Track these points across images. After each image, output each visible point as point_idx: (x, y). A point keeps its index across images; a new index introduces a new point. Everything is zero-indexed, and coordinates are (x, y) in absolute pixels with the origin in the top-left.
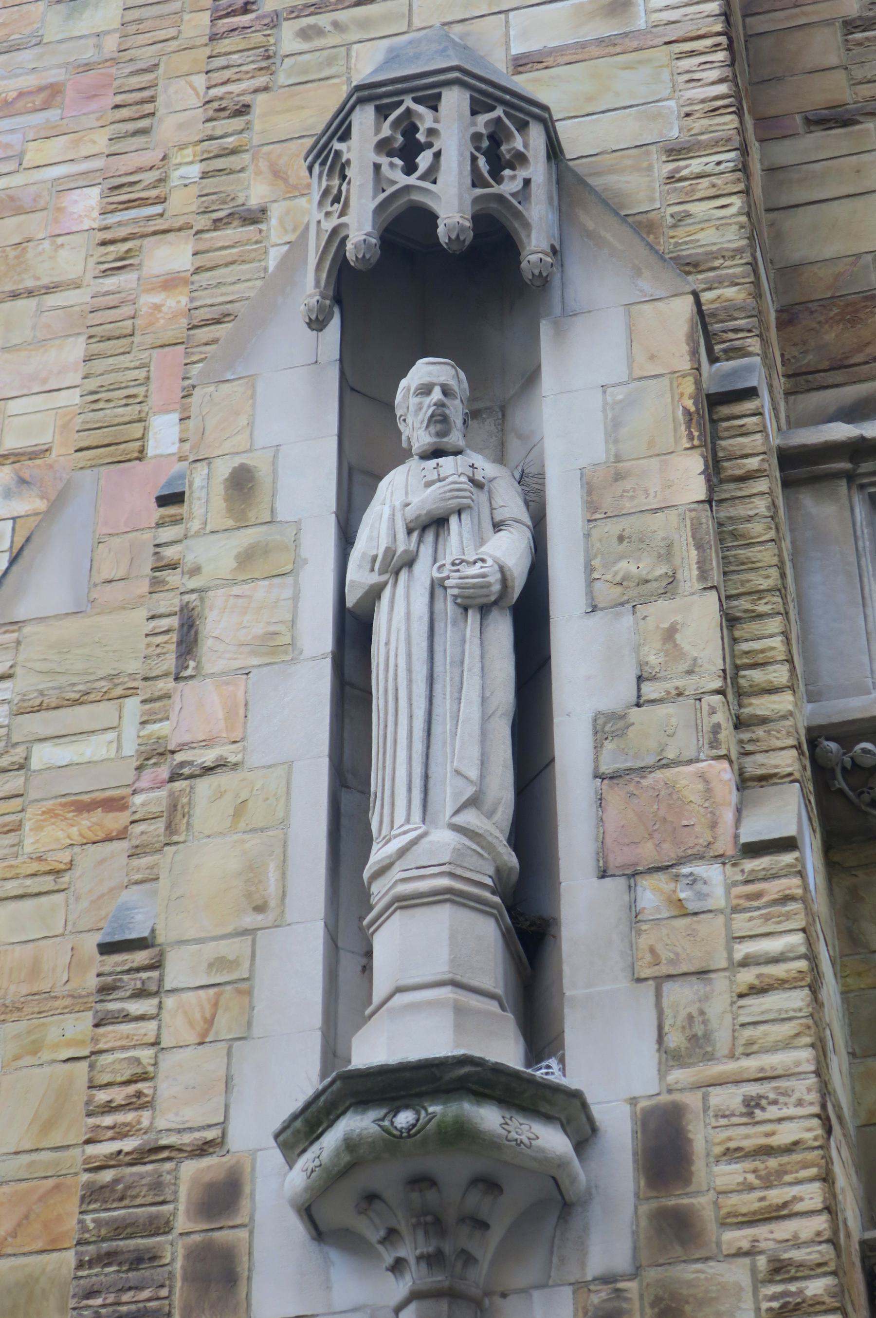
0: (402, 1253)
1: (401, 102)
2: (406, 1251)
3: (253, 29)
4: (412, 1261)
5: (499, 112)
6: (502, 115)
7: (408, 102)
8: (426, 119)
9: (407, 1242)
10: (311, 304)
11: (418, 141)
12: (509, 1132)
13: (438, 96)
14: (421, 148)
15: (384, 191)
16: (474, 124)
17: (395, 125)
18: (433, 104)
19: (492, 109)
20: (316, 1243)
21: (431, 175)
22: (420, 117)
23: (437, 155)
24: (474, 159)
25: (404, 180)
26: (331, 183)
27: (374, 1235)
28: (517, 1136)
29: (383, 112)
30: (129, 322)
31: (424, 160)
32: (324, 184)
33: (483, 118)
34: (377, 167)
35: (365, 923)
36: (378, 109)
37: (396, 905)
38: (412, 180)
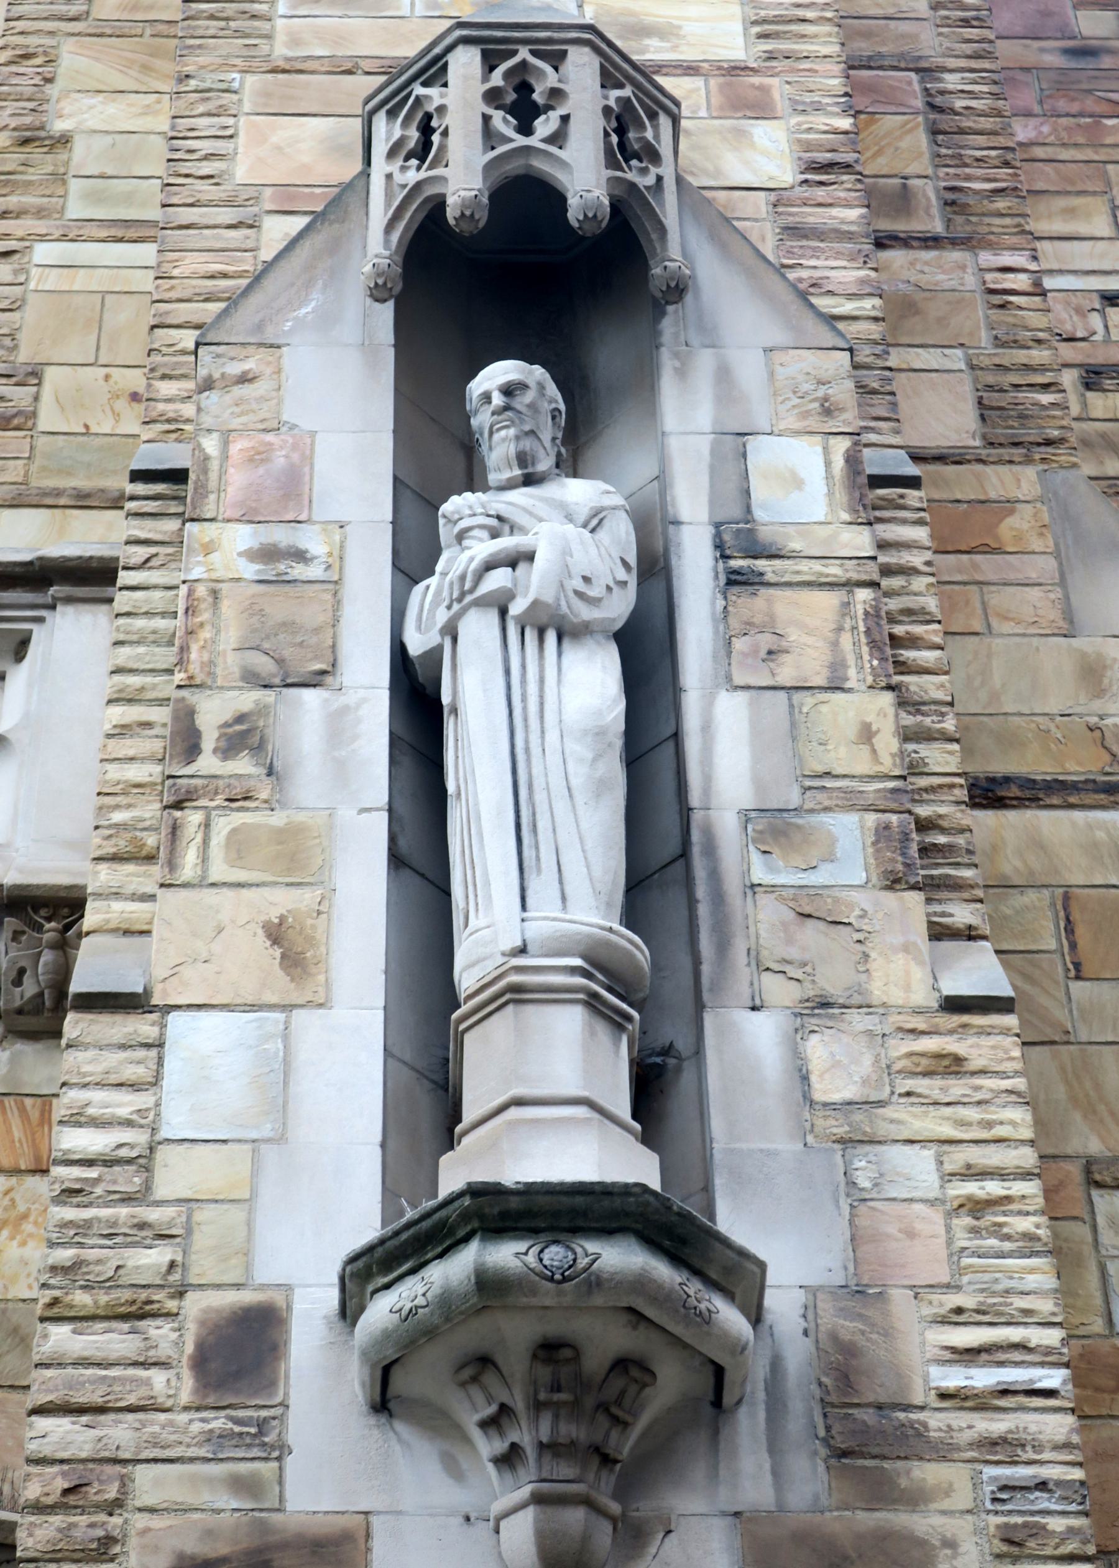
0: (514, 1436)
1: (515, 53)
2: (523, 1435)
3: (14, 380)
4: (530, 1452)
5: (627, 92)
6: (631, 94)
7: (524, 53)
8: (547, 78)
9: (524, 1423)
10: (381, 266)
11: (534, 103)
12: (689, 1296)
13: (563, 54)
14: (536, 111)
15: (493, 148)
16: (606, 97)
17: (507, 75)
18: (555, 64)
19: (621, 86)
20: (372, 1420)
21: (557, 138)
22: (541, 73)
23: (565, 119)
24: (607, 134)
25: (521, 141)
26: (407, 133)
27: (470, 1420)
28: (696, 1303)
29: (490, 62)
30: (52, 1281)
31: (544, 126)
32: (397, 133)
33: (615, 93)
34: (486, 119)
35: (454, 1016)
36: (485, 54)
37: (508, 996)
38: (533, 141)
